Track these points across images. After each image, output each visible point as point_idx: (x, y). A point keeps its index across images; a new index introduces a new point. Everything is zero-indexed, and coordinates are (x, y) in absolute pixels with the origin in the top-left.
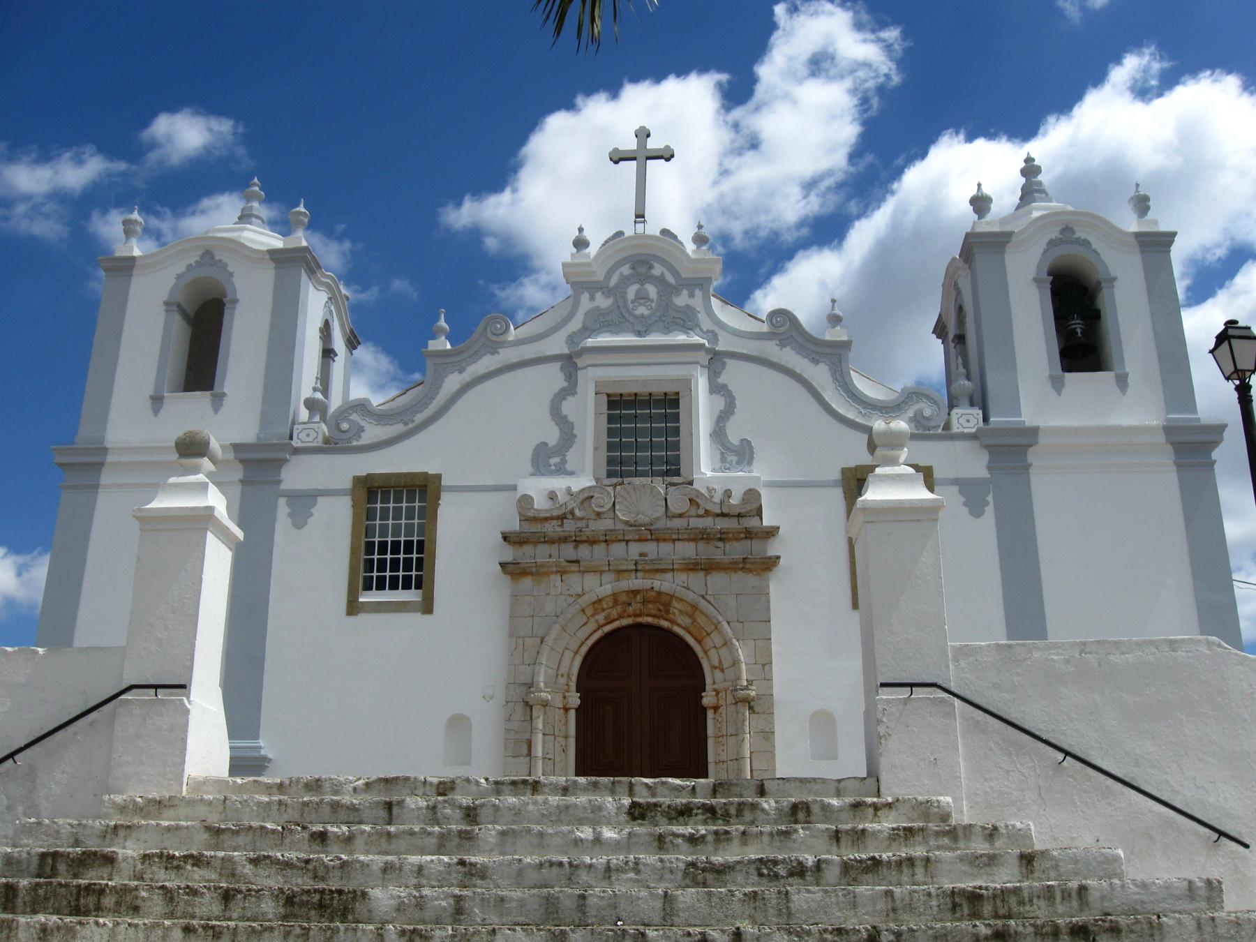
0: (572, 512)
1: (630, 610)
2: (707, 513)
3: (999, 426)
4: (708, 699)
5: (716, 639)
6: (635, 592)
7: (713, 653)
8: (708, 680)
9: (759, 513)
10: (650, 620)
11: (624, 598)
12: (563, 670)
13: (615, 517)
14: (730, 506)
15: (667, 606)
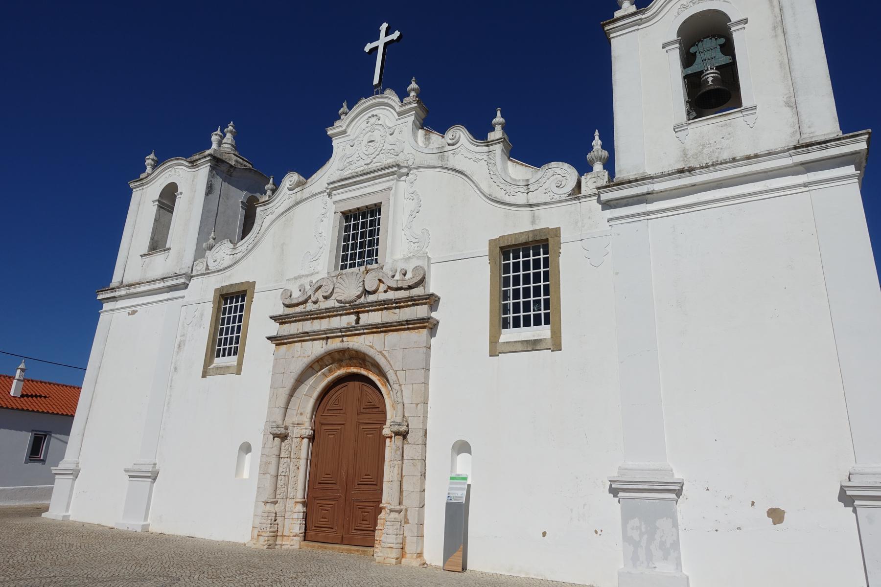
2: (390, 288)
9: (421, 282)
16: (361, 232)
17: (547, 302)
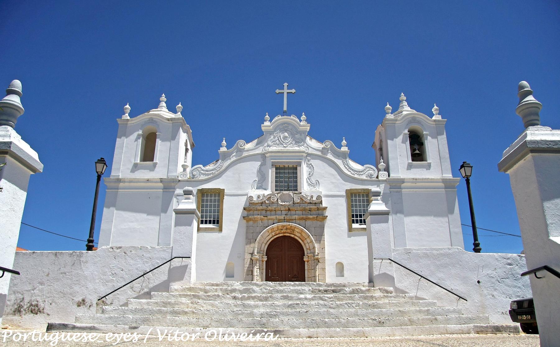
0: (265, 201)
1: (282, 231)
3: (394, 179)
4: (305, 259)
5: (308, 240)
6: (284, 226)
7: (307, 245)
8: (306, 253)
9: (321, 203)
10: (288, 235)
11: (280, 228)
12: (262, 249)
13: (278, 203)
14: (313, 201)
15: (293, 230)
16: (287, 176)
17: (218, 210)
